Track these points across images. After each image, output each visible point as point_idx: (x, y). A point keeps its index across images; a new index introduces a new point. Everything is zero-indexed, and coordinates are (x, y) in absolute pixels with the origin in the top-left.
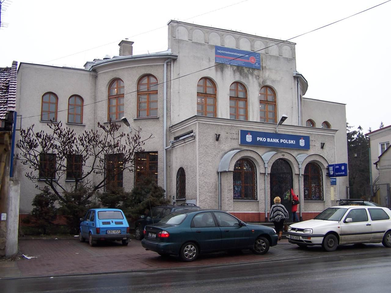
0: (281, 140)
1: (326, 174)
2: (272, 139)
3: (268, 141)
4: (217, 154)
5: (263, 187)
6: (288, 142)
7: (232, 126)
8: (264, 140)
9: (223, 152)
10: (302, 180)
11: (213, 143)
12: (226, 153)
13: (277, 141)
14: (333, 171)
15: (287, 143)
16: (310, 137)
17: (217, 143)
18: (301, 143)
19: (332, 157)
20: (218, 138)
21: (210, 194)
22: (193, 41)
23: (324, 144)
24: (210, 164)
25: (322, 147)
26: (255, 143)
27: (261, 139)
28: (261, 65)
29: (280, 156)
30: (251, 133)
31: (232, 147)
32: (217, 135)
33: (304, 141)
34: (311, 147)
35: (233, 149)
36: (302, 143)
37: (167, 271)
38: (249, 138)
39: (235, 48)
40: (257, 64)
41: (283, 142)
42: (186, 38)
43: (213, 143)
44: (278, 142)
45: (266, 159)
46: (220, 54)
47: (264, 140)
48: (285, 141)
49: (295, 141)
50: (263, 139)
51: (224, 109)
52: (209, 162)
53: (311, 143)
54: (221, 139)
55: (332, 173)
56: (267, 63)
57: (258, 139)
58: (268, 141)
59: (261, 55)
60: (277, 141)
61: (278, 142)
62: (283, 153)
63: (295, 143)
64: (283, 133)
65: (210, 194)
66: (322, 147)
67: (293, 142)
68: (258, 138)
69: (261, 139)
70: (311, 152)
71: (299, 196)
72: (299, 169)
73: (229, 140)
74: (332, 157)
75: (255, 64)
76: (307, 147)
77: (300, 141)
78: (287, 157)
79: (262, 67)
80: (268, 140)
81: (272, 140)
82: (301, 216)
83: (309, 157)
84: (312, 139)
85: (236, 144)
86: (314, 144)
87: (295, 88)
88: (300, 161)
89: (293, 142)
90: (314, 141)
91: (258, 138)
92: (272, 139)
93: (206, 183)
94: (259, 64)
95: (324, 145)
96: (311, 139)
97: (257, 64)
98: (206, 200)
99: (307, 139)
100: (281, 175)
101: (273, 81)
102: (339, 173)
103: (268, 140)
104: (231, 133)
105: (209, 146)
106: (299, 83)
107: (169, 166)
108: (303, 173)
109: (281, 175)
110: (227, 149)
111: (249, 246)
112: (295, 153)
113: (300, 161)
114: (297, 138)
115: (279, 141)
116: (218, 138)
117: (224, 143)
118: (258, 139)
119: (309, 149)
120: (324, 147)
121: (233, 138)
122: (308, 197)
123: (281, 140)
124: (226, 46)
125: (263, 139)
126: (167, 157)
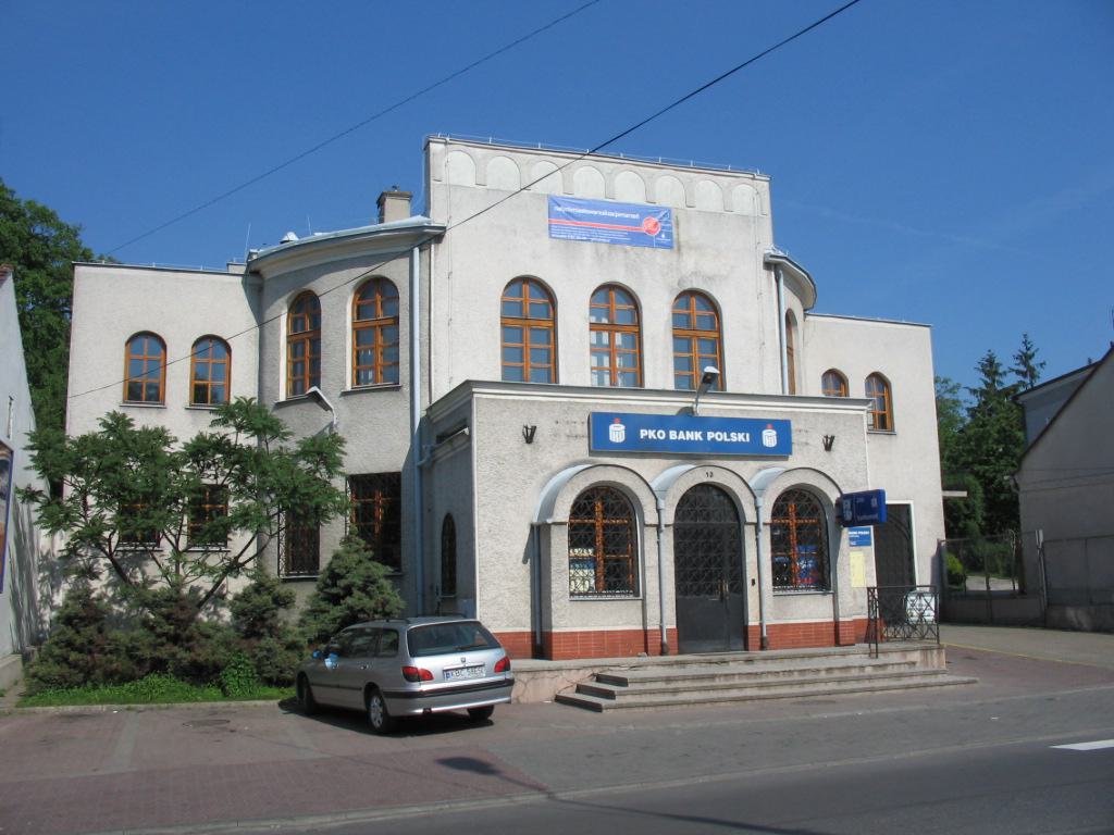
0: (709, 433)
1: (834, 519)
2: (681, 432)
3: (671, 438)
4: (531, 478)
5: (657, 559)
6: (729, 437)
7: (571, 403)
8: (661, 435)
9: (547, 473)
10: (668, 539)
11: (518, 448)
12: (554, 474)
13: (697, 436)
14: (852, 509)
15: (726, 440)
16: (792, 423)
17: (528, 447)
18: (761, 438)
19: (857, 471)
20: (529, 436)
21: (512, 585)
22: (488, 187)
23: (833, 438)
24: (509, 505)
25: (828, 447)
26: (636, 447)
27: (651, 434)
28: (675, 236)
29: (700, 476)
30: (623, 418)
31: (571, 459)
32: (527, 428)
33: (774, 433)
34: (795, 448)
35: (575, 464)
36: (769, 438)
37: (601, 790)
38: (617, 433)
39: (602, 198)
40: (663, 236)
41: (713, 439)
42: (470, 181)
43: (518, 448)
44: (701, 439)
45: (659, 485)
46: (559, 215)
47: (661, 435)
48: (719, 436)
49: (748, 435)
50: (656, 434)
51: (576, 356)
52: (508, 498)
53: (795, 437)
54: (541, 439)
55: (848, 516)
56: (687, 232)
57: (643, 433)
58: (671, 438)
59: (673, 211)
60: (697, 436)
61: (701, 439)
62: (709, 470)
63: (748, 440)
64: (716, 415)
65: (512, 585)
66: (828, 447)
67: (745, 437)
68: (642, 431)
69: (651, 434)
70: (794, 461)
71: (757, 582)
72: (758, 510)
73: (563, 438)
74: (857, 471)
75: (659, 236)
76: (783, 449)
77: (765, 433)
78: (720, 478)
79: (678, 243)
80: (673, 435)
81: (682, 436)
82: (765, 634)
83: (786, 476)
84: (801, 427)
85: (581, 449)
86: (804, 440)
87: (770, 292)
88: (757, 487)
89: (745, 437)
90: (803, 432)
91: (642, 431)
92: (681, 432)
93: (501, 554)
94: (669, 235)
95: (831, 442)
96: (794, 426)
97: (663, 236)
98: (500, 599)
99: (783, 428)
100: (708, 528)
101: (711, 278)
102: (865, 517)
103: (673, 435)
104: (568, 422)
105: (507, 458)
106: (782, 281)
107: (427, 509)
108: (769, 520)
109: (708, 528)
110: (556, 464)
111: (814, 716)
112: (747, 468)
113: (757, 487)
114: (755, 426)
115: (704, 436)
116: (529, 436)
117: (549, 449)
118: (643, 433)
119: (791, 453)
120: (833, 447)
121: (574, 433)
122: (784, 577)
123: (709, 433)
124: (578, 195)
125: (656, 434)
126: (421, 485)
